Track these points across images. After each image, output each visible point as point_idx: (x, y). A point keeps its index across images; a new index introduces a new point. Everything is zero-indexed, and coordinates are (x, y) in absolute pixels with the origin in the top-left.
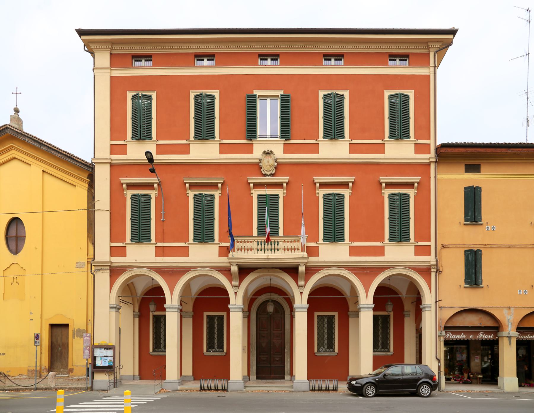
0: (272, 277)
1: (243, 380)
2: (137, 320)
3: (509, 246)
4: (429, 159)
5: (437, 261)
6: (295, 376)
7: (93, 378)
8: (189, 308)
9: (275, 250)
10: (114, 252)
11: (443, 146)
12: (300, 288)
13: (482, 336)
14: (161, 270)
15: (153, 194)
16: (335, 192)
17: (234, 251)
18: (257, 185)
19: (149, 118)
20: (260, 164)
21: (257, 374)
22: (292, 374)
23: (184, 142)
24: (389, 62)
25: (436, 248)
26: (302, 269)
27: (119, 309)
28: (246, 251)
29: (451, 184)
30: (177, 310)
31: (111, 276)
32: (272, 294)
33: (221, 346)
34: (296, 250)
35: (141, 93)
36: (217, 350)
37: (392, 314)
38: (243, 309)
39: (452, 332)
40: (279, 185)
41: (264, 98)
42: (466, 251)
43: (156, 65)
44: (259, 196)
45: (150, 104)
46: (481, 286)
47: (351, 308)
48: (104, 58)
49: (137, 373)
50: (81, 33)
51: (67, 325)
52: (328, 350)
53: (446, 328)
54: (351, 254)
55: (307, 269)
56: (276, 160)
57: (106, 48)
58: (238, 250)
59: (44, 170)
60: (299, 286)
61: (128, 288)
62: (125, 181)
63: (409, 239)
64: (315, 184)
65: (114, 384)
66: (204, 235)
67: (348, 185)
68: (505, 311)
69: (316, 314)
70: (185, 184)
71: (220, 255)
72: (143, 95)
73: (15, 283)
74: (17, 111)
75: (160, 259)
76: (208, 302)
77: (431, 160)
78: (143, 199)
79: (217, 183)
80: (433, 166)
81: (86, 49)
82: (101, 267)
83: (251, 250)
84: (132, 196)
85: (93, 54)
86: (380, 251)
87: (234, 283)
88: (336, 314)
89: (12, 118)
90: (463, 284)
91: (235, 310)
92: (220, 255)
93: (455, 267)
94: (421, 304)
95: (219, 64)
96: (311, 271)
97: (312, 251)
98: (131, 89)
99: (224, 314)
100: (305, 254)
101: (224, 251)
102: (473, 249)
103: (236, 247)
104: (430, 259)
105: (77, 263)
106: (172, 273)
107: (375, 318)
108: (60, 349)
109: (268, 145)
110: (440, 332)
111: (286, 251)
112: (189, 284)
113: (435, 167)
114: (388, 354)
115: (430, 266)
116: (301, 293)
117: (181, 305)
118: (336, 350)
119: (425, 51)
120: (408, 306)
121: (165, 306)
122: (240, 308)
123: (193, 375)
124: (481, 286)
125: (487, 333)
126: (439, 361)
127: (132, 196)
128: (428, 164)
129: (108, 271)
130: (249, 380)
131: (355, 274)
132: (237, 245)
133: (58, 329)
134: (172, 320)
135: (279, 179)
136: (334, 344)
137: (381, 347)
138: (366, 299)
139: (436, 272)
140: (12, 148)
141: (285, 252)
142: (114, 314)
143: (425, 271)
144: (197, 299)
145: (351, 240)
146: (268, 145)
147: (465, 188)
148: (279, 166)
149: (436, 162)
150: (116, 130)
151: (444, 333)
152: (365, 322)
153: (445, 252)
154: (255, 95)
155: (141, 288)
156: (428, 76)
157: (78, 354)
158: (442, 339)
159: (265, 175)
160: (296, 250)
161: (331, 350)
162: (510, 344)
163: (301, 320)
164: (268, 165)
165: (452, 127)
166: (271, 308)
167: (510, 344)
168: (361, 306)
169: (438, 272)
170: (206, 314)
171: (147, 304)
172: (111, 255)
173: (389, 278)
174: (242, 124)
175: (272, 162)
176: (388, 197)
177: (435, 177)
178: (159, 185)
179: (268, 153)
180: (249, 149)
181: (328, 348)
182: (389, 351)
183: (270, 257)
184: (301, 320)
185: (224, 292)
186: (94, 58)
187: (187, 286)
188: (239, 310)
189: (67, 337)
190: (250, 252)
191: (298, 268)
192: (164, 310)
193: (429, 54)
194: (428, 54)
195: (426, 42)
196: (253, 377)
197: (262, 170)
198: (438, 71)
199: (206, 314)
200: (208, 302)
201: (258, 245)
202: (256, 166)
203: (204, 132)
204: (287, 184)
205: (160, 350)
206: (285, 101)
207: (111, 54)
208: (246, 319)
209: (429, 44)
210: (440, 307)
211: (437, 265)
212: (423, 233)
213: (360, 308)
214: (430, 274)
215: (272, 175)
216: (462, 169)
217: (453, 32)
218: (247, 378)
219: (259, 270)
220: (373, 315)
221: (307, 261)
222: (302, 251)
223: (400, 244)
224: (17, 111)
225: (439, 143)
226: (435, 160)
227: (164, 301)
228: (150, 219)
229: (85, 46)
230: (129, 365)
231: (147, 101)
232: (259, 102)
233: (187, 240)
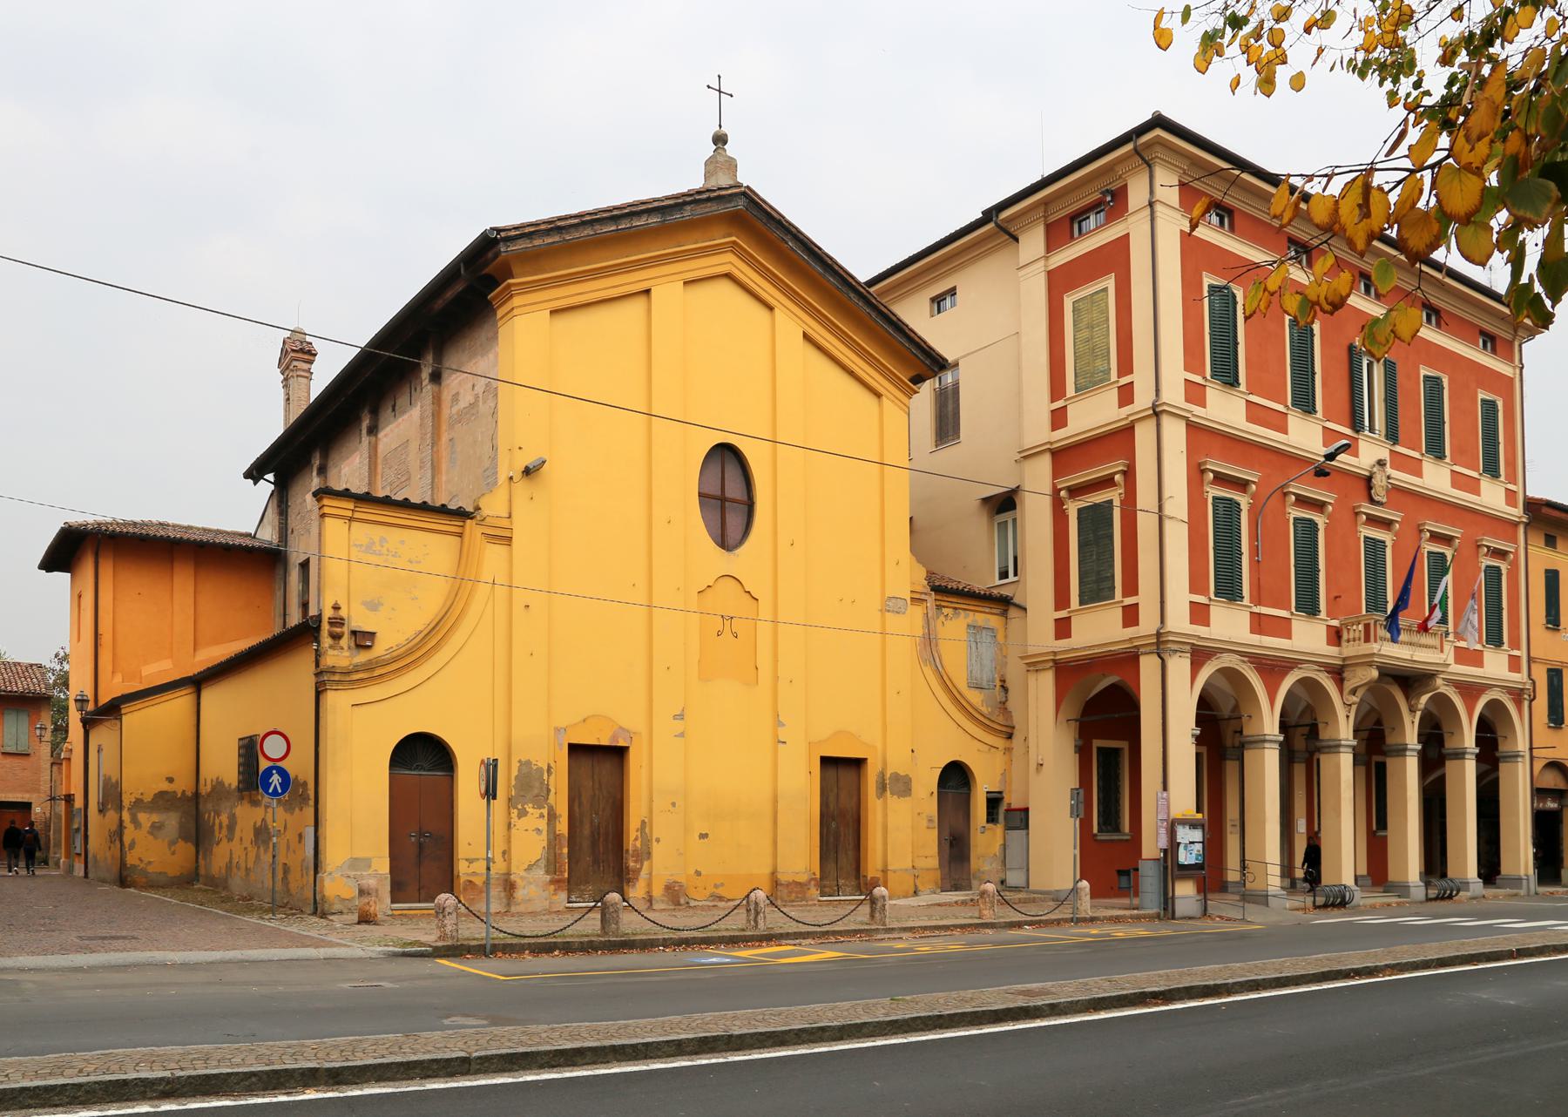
38: (1354, 748)
59: (810, 332)
73: (727, 634)
74: (720, 140)
75: (1256, 639)
98: (1213, 272)
108: (833, 825)
119: (1508, 337)
128: (1516, 524)
131: (1461, 694)
133: (841, 771)
195: (1109, 168)
224: (720, 140)
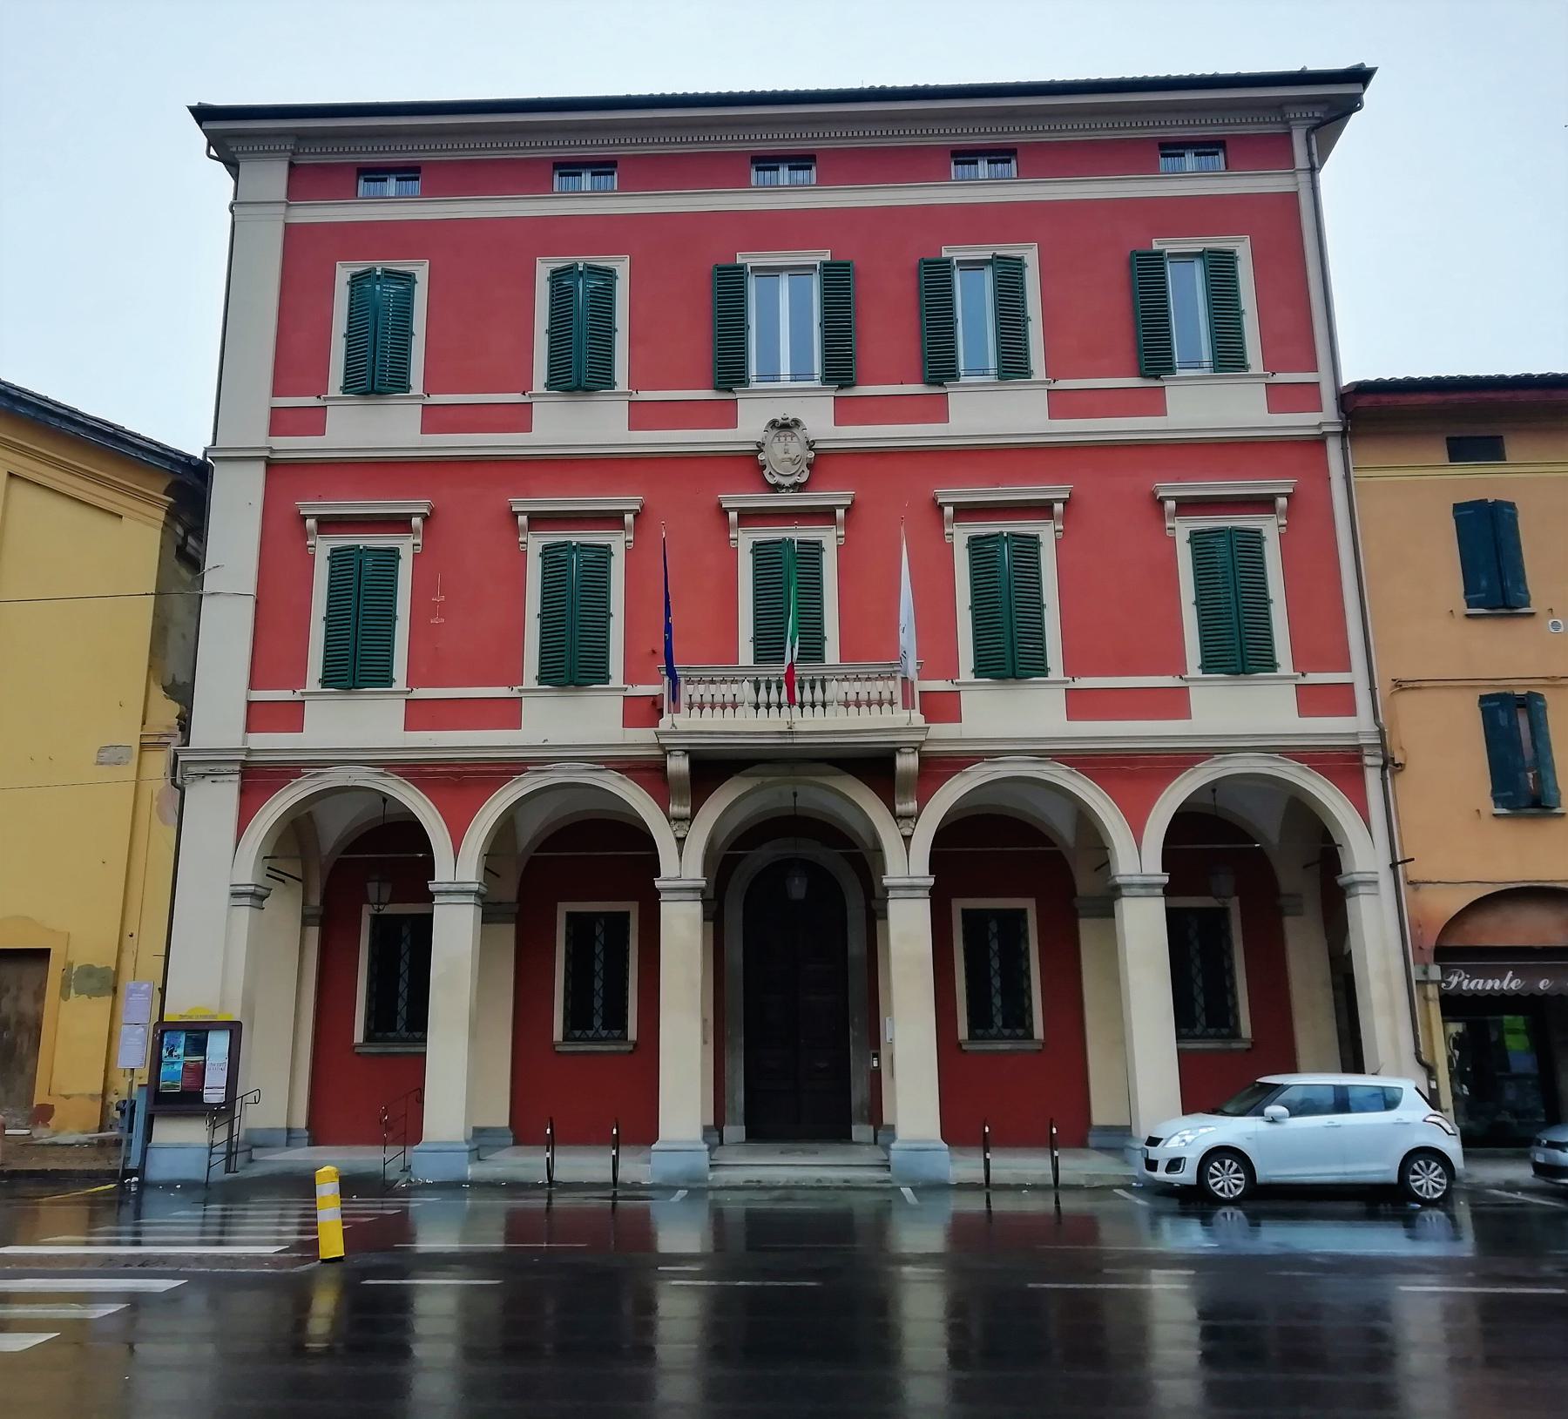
0: (799, 789)
1: (705, 1139)
2: (314, 932)
4: (1319, 426)
5: (1381, 733)
6: (892, 1128)
7: (148, 1136)
9: (813, 705)
10: (257, 715)
11: (1362, 388)
12: (902, 823)
14: (419, 772)
16: (1006, 530)
17: (677, 710)
18: (749, 517)
19: (406, 333)
20: (761, 457)
21: (748, 1122)
22: (874, 1114)
23: (516, 398)
24: (1162, 160)
25: (1372, 690)
26: (907, 763)
28: (696, 710)
29: (1402, 508)
30: (472, 899)
31: (243, 792)
33: (617, 1020)
34: (886, 706)
35: (379, 266)
36: (604, 1033)
37: (1234, 905)
40: (825, 515)
41: (776, 271)
42: (1483, 699)
43: (430, 192)
44: (757, 546)
45: (408, 296)
46: (1558, 810)
47: (1085, 884)
48: (271, 177)
49: (301, 1121)
50: (203, 114)
51: (42, 955)
52: (1007, 1032)
54: (1073, 714)
55: (925, 760)
56: (810, 445)
57: (280, 151)
59: (15, 470)
60: (898, 817)
61: (296, 832)
62: (312, 508)
63: (1272, 666)
64: (940, 508)
65: (228, 1159)
66: (573, 663)
67: (1052, 507)
69: (958, 905)
70: (516, 515)
71: (628, 721)
72: (386, 272)
76: (575, 876)
77: (1326, 429)
78: (369, 563)
79: (623, 512)
80: (1333, 447)
81: (213, 152)
82: (212, 766)
83: (735, 706)
84: (333, 551)
85: (233, 167)
86: (1175, 703)
87: (675, 809)
88: (1029, 905)
90: (1489, 806)
91: (901, 893)
92: (628, 721)
93: (1448, 756)
95: (628, 186)
96: (937, 767)
97: (941, 707)
99: (632, 908)
100: (918, 718)
101: (644, 712)
102: (1507, 691)
103: (684, 699)
104: (1356, 726)
105: (103, 749)
106: (459, 783)
107: (1175, 919)
109: (786, 405)
110: (1420, 968)
111: (853, 709)
113: (1344, 449)
114: (1235, 1045)
115: (1359, 747)
116: (907, 839)
118: (1039, 1031)
119: (1279, 129)
120: (1292, 878)
122: (694, 889)
124: (1558, 810)
126: (1430, 1071)
127: (333, 551)
128: (1319, 442)
129: (237, 777)
130: (721, 1143)
132: (686, 691)
134: (456, 934)
135: (824, 497)
136: (1028, 1011)
137: (1203, 1019)
138: (1137, 855)
139: (1384, 768)
141: (843, 713)
142: (244, 914)
143: (1343, 765)
144: (339, 863)
145: (1071, 669)
146: (786, 405)
147: (1457, 507)
148: (823, 462)
149: (1343, 434)
150: (294, 364)
151: (1435, 972)
152: (1142, 928)
153: (1405, 699)
154: (742, 267)
155: (334, 828)
156: (1294, 196)
158: (1432, 991)
159: (776, 488)
160: (886, 706)
161: (1020, 1032)
163: (908, 929)
164: (784, 459)
165: (1382, 330)
166: (798, 888)
169: (1390, 766)
170: (563, 909)
171: (354, 883)
172: (249, 728)
173: (1213, 787)
174: (699, 343)
175: (796, 448)
176: (1190, 541)
177: (1347, 477)
180: (725, 415)
181: (1005, 1026)
182: (1235, 1035)
183: (797, 728)
184: (908, 929)
185: (644, 840)
186: (236, 177)
187: (506, 827)
188: (691, 896)
189: (40, 995)
190: (729, 710)
191: (893, 760)
192: (429, 898)
193: (1289, 135)
194: (1288, 136)
195: (1280, 105)
196: (735, 1132)
197: (766, 473)
198: (1325, 176)
199: (563, 909)
200: (575, 876)
201: (757, 690)
202: (749, 464)
203: (580, 372)
204: (848, 509)
205: (391, 1035)
206: (836, 280)
207: (291, 165)
209: (1286, 109)
210: (1411, 883)
211: (1383, 745)
212: (1322, 643)
214: (1359, 773)
216: (1442, 455)
217: (1361, 76)
218: (714, 1132)
220: (1168, 910)
221: (923, 738)
222: (905, 707)
223: (1242, 681)
225: (1346, 380)
226: (1340, 429)
228: (391, 617)
229: (209, 145)
230: (275, 1090)
231: (394, 288)
232: (752, 285)
233: (516, 678)
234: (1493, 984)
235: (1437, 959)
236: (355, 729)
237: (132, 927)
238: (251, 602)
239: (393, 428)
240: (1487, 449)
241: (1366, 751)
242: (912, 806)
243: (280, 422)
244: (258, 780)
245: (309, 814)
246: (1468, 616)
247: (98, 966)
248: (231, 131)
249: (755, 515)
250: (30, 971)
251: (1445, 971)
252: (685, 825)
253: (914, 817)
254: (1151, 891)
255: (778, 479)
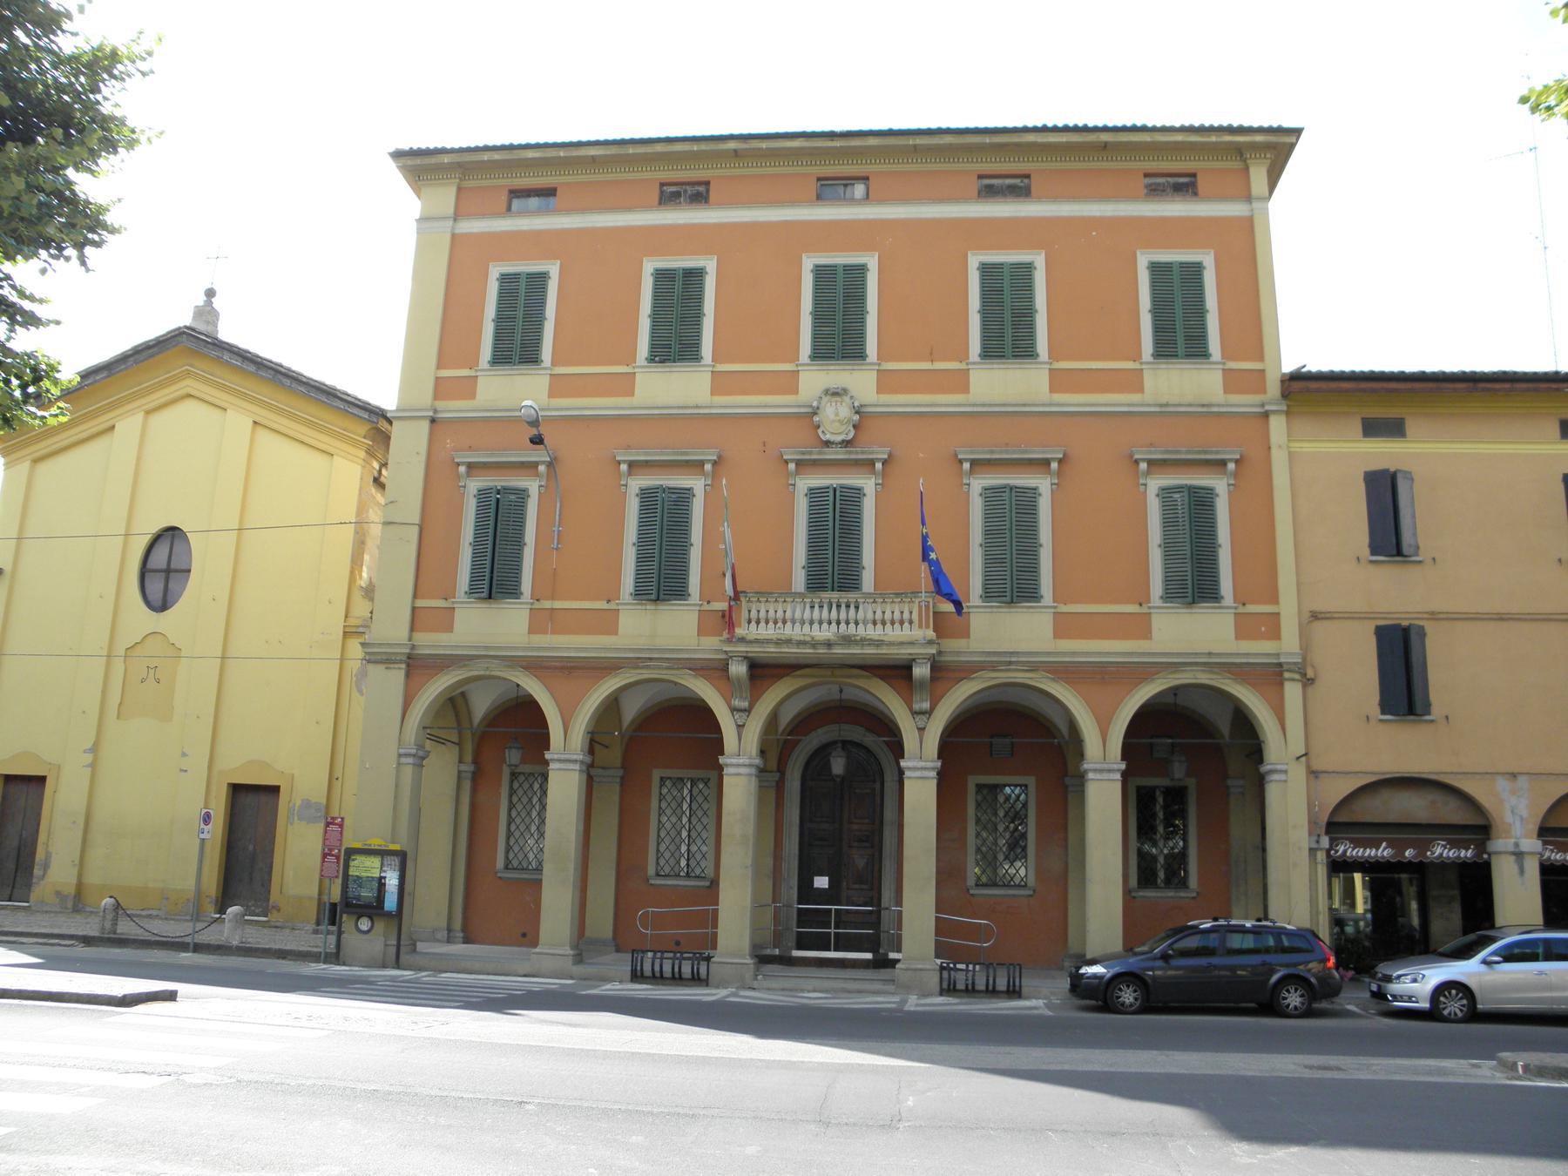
3: (1501, 618)
4: (1263, 405)
8: (615, 755)
11: (1298, 377)
13: (1440, 851)
15: (533, 486)
26: (921, 671)
27: (423, 758)
31: (408, 675)
32: (845, 727)
39: (1352, 841)
48: (445, 197)
51: (275, 790)
53: (1335, 828)
58: (749, 622)
59: (258, 419)
60: (915, 713)
61: (455, 703)
68: (1502, 784)
74: (210, 293)
80: (1277, 425)
87: (737, 703)
89: (199, 313)
93: (1354, 670)
94: (1261, 760)
96: (943, 672)
99: (713, 775)
112: (616, 699)
116: (921, 730)
117: (591, 751)
121: (548, 756)
123: (614, 938)
125: (1454, 844)
140: (188, 374)
143: (1271, 675)
151: (1325, 842)
152: (1104, 802)
153: (1319, 628)
155: (482, 704)
157: (298, 857)
158: (1321, 856)
159: (827, 443)
162: (1522, 871)
166: (838, 766)
167: (1522, 871)
168: (1086, 766)
173: (1175, 691)
175: (845, 411)
178: (550, 465)
179: (836, 394)
187: (612, 706)
192: (547, 763)
207: (459, 189)
208: (772, 794)
213: (1086, 771)
215: (846, 443)
216: (1357, 427)
219: (807, 671)
222: (920, 626)
227: (544, 741)
234: (1370, 853)
235: (1327, 833)
236: (499, 628)
237: (338, 773)
238: (416, 529)
239: (524, 392)
240: (1394, 429)
241: (1286, 675)
242: (926, 705)
243: (442, 388)
244: (416, 666)
245: (463, 694)
246: (41, 301)
247: (314, 801)
248: (420, 165)
249: (562, 668)
250: (264, 798)
251: (1334, 842)
252: (744, 715)
253: (929, 713)
254: (1105, 776)
255: (828, 437)
